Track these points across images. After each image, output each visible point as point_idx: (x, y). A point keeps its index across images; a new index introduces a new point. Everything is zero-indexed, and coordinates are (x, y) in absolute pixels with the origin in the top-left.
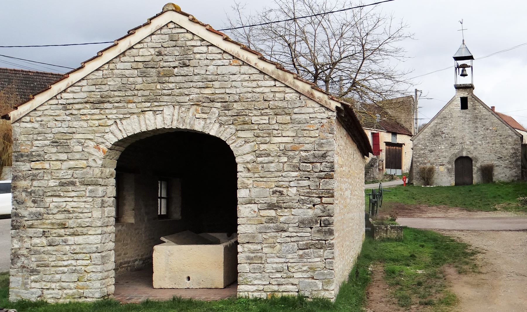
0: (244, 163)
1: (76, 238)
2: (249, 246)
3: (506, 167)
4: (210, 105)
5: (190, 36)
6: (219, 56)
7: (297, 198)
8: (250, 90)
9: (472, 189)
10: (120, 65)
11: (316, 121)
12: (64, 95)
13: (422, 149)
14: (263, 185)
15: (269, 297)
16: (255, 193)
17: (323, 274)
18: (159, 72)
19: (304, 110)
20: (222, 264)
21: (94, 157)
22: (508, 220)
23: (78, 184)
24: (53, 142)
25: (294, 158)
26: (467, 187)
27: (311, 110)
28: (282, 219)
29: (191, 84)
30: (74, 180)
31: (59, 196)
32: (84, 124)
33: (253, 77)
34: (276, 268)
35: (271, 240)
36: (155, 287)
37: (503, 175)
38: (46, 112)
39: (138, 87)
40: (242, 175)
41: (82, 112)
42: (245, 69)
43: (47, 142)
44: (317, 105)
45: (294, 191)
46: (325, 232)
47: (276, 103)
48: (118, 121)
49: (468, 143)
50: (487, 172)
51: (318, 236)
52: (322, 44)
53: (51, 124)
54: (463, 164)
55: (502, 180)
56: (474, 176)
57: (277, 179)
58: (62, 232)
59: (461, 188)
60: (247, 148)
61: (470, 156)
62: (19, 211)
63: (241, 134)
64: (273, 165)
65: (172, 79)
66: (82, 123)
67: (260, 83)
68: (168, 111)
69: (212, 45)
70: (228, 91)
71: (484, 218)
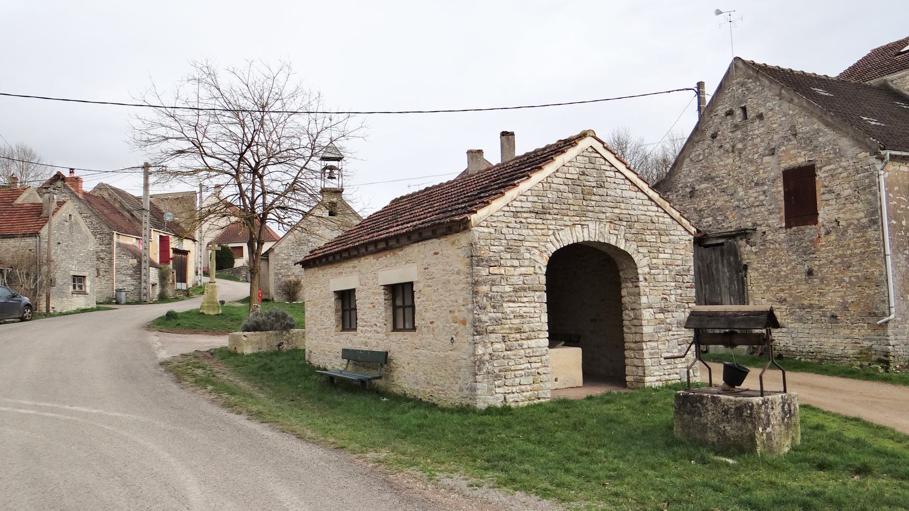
5: (603, 160)
10: (555, 180)
13: (285, 259)
31: (514, 302)
43: (502, 248)
45: (673, 297)
53: (505, 230)
58: (518, 336)
63: (641, 249)
65: (593, 198)
67: (650, 208)
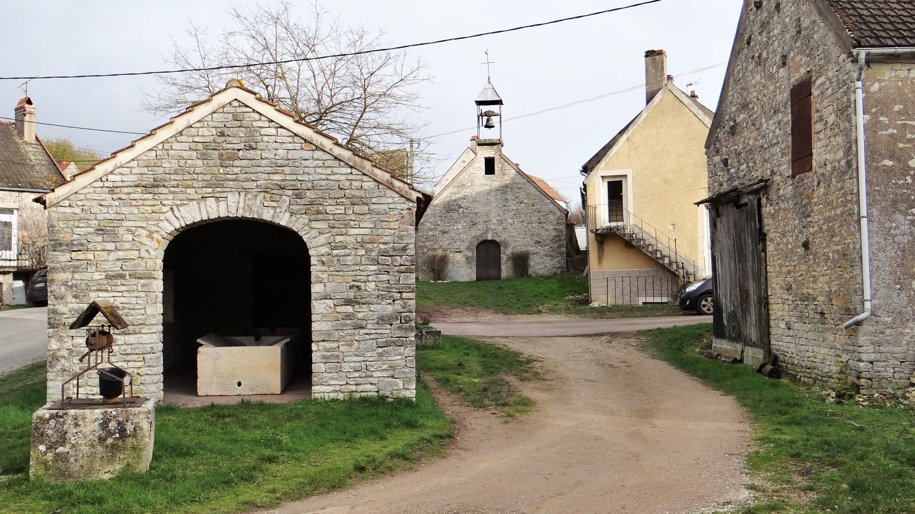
0: (318, 256)
1: (127, 338)
2: (325, 344)
3: (546, 255)
4: (281, 192)
5: (257, 116)
6: (290, 139)
7: (376, 293)
8: (324, 177)
9: (502, 285)
10: (176, 146)
11: (396, 212)
12: (111, 177)
13: (431, 230)
14: (339, 279)
15: (347, 399)
16: (330, 287)
17: (404, 373)
18: (222, 155)
19: (383, 200)
20: (279, 368)
21: (147, 248)
22: (560, 325)
23: (128, 277)
24: (98, 230)
25: (372, 251)
26: (495, 282)
27: (390, 201)
28: (360, 315)
29: (259, 169)
30: (124, 273)
31: (106, 291)
32: (135, 210)
33: (328, 163)
34: (354, 368)
35: (348, 338)
36: (199, 394)
37: (542, 266)
38: (89, 196)
39: (198, 170)
40: (316, 269)
41: (132, 196)
42: (318, 154)
43: (91, 230)
44: (396, 195)
46: (406, 329)
47: (353, 192)
48: (175, 208)
49: (494, 221)
50: (521, 261)
51: (399, 333)
52: (306, 82)
53: (96, 209)
54: (487, 251)
55: (541, 272)
56: (503, 267)
57: (354, 273)
59: (486, 283)
60: (322, 239)
61: (497, 239)
62: (57, 307)
63: (314, 224)
64: (349, 258)
65: (237, 163)
66: (133, 209)
68: (232, 198)
69: (282, 127)
70: (300, 178)
71: (528, 323)
